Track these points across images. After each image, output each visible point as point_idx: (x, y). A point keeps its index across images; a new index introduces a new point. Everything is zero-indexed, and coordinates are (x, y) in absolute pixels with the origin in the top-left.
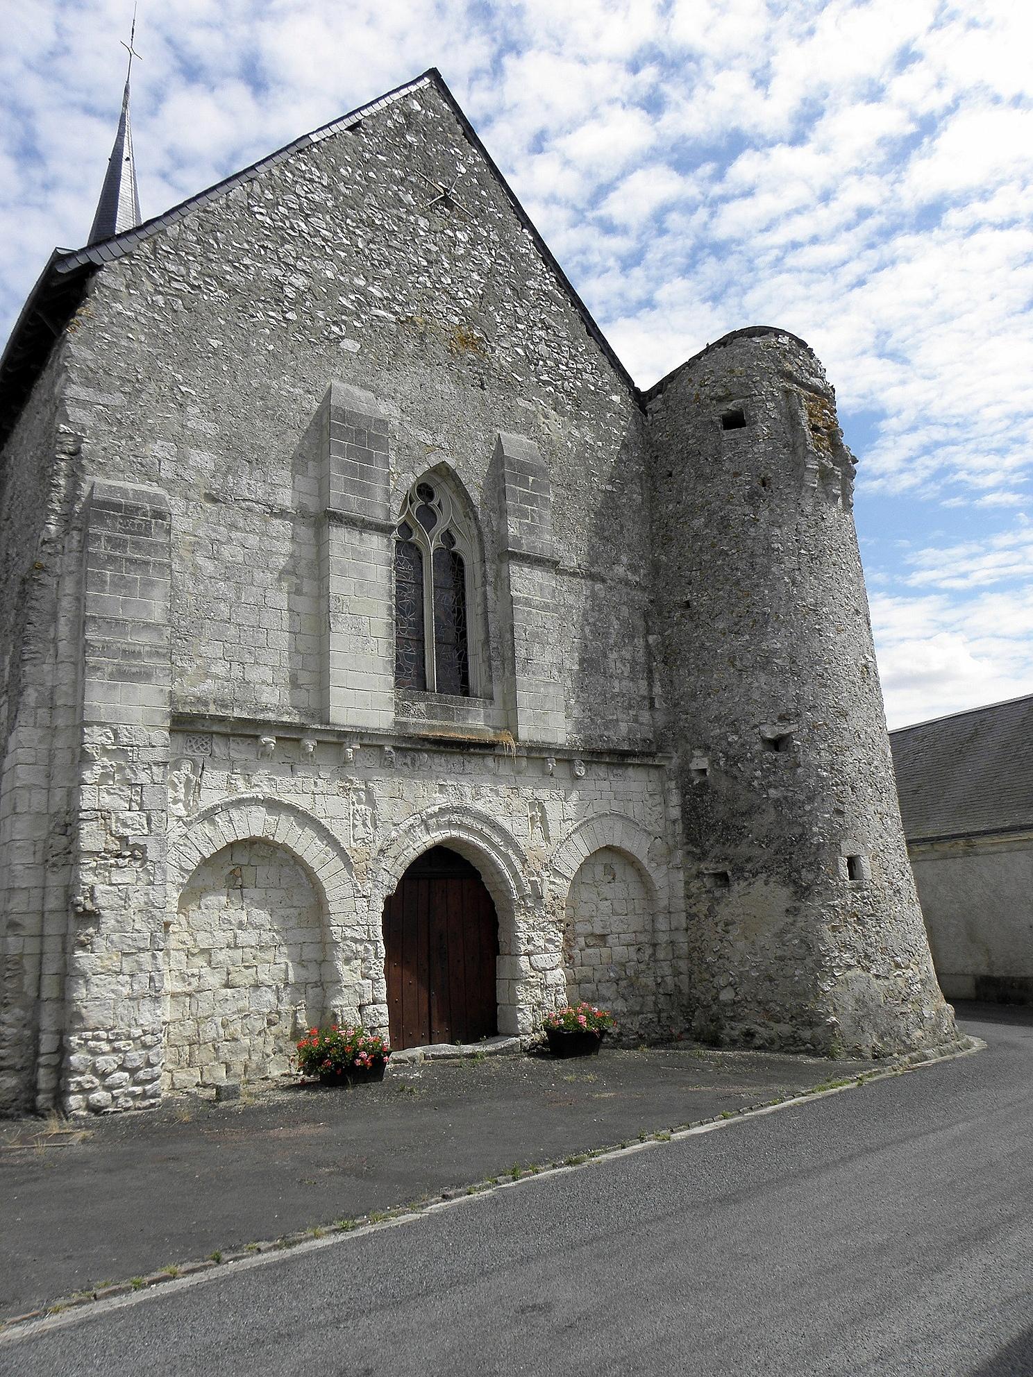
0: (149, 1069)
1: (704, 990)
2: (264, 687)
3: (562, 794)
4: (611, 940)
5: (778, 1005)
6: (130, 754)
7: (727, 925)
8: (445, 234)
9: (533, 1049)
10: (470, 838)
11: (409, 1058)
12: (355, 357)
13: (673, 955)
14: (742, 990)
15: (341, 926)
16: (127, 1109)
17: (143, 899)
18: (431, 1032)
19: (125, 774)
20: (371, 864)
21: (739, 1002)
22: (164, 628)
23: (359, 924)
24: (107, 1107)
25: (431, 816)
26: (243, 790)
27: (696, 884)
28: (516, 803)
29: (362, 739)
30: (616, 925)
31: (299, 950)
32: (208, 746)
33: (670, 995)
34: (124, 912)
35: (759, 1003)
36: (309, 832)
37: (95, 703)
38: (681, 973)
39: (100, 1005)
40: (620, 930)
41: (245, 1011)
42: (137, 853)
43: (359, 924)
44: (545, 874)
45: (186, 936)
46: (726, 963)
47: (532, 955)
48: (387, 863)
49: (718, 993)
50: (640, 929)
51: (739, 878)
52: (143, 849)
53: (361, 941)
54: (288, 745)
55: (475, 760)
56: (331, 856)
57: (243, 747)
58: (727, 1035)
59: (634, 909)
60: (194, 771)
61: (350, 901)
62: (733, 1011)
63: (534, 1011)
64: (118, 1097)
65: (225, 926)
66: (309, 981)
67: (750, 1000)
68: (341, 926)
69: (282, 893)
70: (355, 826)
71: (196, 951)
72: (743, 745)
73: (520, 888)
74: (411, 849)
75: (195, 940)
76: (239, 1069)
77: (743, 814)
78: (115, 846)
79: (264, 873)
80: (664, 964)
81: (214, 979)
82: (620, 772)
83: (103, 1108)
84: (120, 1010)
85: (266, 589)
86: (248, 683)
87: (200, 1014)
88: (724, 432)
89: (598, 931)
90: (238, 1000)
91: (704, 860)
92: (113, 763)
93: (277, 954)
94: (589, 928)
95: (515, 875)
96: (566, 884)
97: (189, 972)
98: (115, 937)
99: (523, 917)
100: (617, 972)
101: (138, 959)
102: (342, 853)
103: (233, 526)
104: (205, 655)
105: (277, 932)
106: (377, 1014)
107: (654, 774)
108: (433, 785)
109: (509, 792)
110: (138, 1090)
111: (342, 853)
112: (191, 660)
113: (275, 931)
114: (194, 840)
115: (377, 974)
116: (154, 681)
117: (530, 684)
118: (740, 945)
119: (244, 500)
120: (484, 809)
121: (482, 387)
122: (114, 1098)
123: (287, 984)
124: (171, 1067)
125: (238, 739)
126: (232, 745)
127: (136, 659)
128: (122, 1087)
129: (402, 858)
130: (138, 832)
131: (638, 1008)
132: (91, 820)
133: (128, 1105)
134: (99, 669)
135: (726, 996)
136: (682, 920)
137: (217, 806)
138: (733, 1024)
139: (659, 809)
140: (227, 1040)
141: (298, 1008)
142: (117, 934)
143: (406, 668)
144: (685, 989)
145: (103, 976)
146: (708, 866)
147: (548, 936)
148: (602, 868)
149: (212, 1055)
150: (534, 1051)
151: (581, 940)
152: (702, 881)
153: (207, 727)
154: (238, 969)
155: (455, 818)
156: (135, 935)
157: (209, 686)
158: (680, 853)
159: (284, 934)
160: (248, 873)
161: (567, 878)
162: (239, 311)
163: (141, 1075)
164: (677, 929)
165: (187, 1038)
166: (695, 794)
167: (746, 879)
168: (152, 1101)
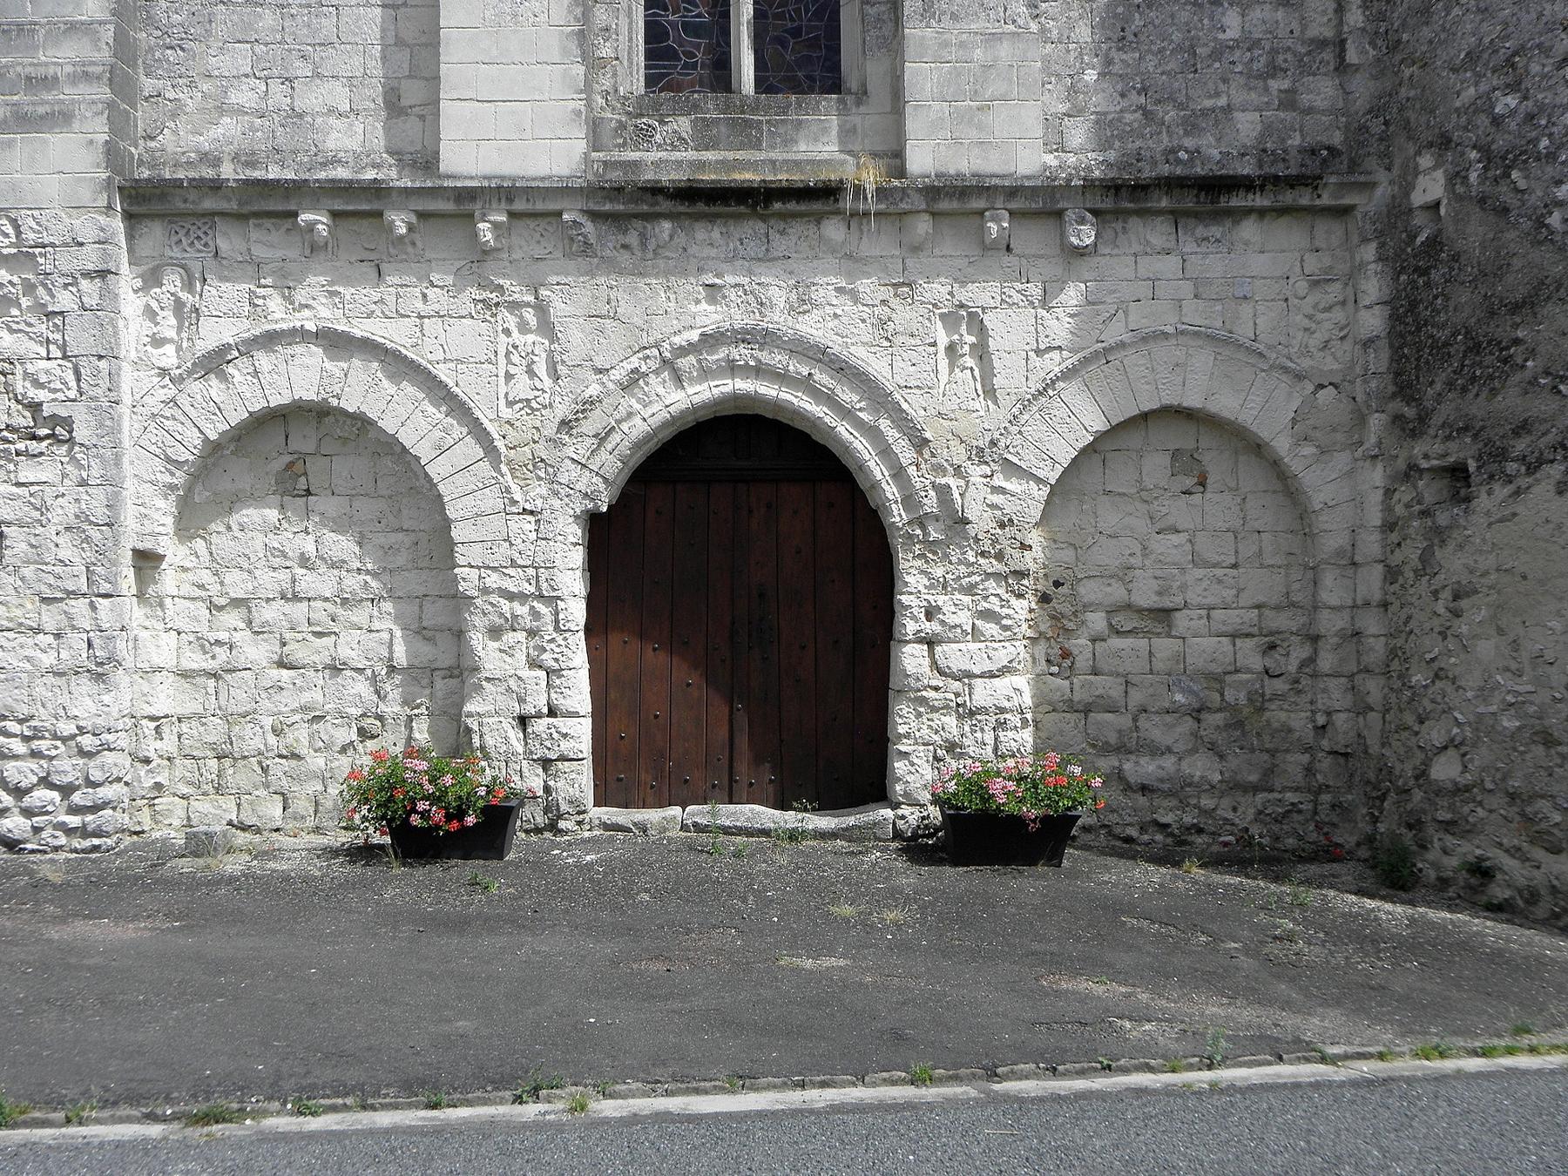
0: (90, 790)
1: (1402, 751)
2: (332, 121)
3: (1035, 290)
4: (1181, 621)
5: (1557, 807)
6: (41, 260)
7: (1456, 597)
9: (930, 836)
10: (783, 396)
11: (635, 824)
14: (1481, 757)
15: (479, 568)
16: (56, 849)
17: (72, 509)
18: (731, 781)
19: (36, 297)
20: (542, 451)
21: (1468, 789)
23: (514, 564)
24: (25, 841)
25: (682, 351)
26: (278, 316)
27: (1404, 494)
28: (904, 316)
29: (510, 200)
30: (1199, 587)
32: (208, 239)
33: (1346, 755)
34: (39, 530)
35: (1513, 797)
36: (409, 388)
39: (7, 680)
40: (1210, 600)
41: (315, 709)
42: (56, 431)
43: (514, 564)
44: (976, 472)
45: (206, 577)
46: (1450, 689)
47: (940, 642)
48: (576, 448)
49: (1427, 763)
51: (1491, 477)
52: (68, 423)
53: (522, 597)
54: (353, 225)
55: (797, 229)
57: (276, 236)
58: (1432, 864)
59: (1260, 553)
60: (189, 286)
61: (497, 522)
62: (1451, 808)
63: (937, 759)
64: (41, 829)
65: (277, 562)
66: (437, 665)
67: (1489, 786)
68: (479, 568)
70: (509, 377)
71: (222, 601)
72: (1530, 117)
73: (909, 500)
74: (637, 420)
75: (222, 583)
76: (302, 805)
77: (1516, 308)
78: (24, 420)
79: (347, 468)
80: (1332, 683)
81: (257, 652)
82: (1215, 231)
83: (20, 842)
84: (40, 691)
86: (300, 116)
87: (232, 708)
89: (1145, 596)
90: (301, 689)
91: (1422, 433)
92: (15, 279)
93: (376, 613)
94: (1117, 593)
95: (899, 473)
96: (1035, 492)
97: (212, 637)
98: (28, 572)
99: (918, 563)
100: (1192, 692)
101: (65, 608)
102: (478, 431)
104: (216, 73)
105: (375, 575)
106: (555, 735)
107: (1329, 232)
108: (691, 286)
109: (886, 293)
110: (74, 821)
111: (478, 431)
113: (368, 572)
114: (188, 409)
115: (556, 660)
116: (76, 126)
117: (946, 44)
118: (1486, 649)
120: (820, 333)
122: (37, 830)
123: (392, 669)
124: (185, 790)
125: (268, 223)
126: (255, 235)
127: (49, 90)
128: (47, 813)
129: (616, 438)
130: (60, 396)
131: (1253, 778)
133: (57, 843)
135: (1445, 770)
136: (1371, 582)
137: (226, 348)
138: (1450, 841)
139: (1339, 315)
140: (281, 756)
141: (416, 711)
142: (32, 567)
144: (1375, 749)
145: (11, 635)
146: (1429, 450)
148: (1165, 459)
149: (259, 778)
150: (917, 848)
151: (1097, 621)
152: (1415, 487)
153: (193, 202)
154: (300, 637)
155: (741, 353)
156: (58, 569)
157: (227, 130)
158: (1376, 422)
159: (386, 577)
160: (315, 466)
161: (1039, 480)
163: (77, 798)
164: (1367, 604)
165: (212, 746)
167: (1509, 480)
168: (96, 841)
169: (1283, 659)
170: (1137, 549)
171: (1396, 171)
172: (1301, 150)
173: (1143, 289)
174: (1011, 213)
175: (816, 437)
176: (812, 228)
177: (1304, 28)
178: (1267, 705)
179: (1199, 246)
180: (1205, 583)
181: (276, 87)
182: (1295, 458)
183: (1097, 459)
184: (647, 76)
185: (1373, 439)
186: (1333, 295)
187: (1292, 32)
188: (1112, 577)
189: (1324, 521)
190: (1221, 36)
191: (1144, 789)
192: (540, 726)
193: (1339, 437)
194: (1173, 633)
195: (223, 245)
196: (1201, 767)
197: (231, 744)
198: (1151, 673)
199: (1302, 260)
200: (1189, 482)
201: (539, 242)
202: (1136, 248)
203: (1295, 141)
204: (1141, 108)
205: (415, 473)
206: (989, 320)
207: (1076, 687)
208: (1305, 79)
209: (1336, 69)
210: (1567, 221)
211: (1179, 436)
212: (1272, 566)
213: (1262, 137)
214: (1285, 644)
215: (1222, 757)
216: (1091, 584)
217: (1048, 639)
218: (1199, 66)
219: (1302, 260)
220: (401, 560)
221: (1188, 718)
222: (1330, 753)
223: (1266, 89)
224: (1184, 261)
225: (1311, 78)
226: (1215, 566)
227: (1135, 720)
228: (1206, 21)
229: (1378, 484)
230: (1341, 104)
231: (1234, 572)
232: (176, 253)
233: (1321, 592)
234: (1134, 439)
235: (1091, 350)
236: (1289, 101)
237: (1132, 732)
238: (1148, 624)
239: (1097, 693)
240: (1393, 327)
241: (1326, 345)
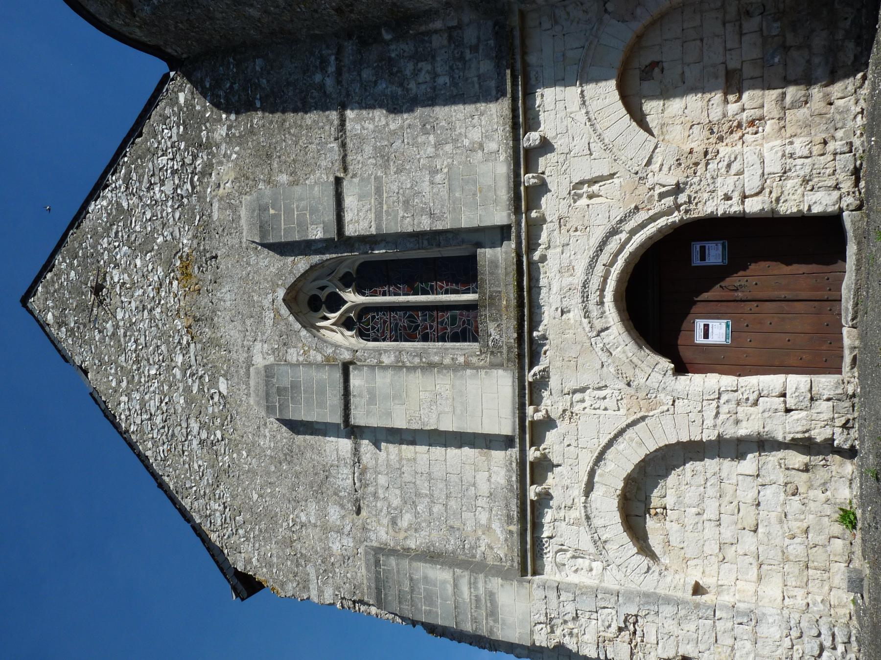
2: (493, 480)
4: (733, 65)
8: (120, 293)
12: (229, 382)
15: (702, 429)
17: (670, 621)
20: (642, 395)
22: (456, 574)
37: (517, 635)
44: (651, 180)
56: (634, 435)
73: (668, 212)
78: (626, 635)
81: (749, 542)
85: (416, 473)
86: (491, 494)
90: (769, 523)
95: (653, 219)
103: (375, 495)
112: (478, 539)
114: (622, 560)
119: (355, 484)
121: (216, 257)
124: (827, 588)
132: (606, 652)
134: (491, 629)
143: (463, 325)
147: (723, 171)
155: (594, 298)
162: (229, 476)
163: (828, 643)
165: (801, 572)
223: (470, 60)
236: (474, 49)
241: (586, 12)
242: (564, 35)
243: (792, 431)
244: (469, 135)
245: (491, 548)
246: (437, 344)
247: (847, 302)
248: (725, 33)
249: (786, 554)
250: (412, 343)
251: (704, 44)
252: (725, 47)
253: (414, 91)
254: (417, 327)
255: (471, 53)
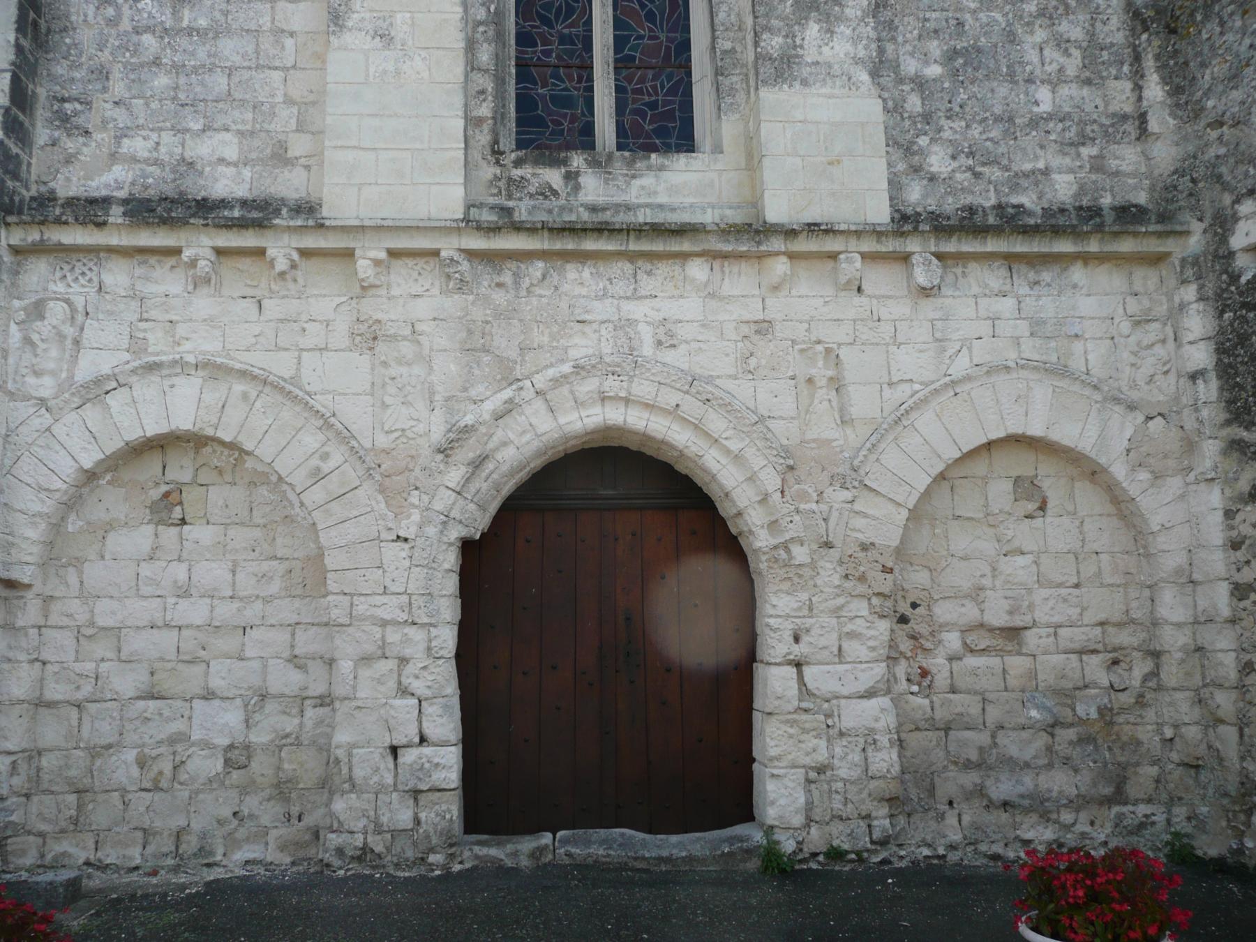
2: (222, 169)
13: (1204, 678)
15: (350, 594)
31: (288, 636)
38: (1222, 721)
40: (1056, 619)
47: (808, 663)
50: (1117, 617)
66: (310, 693)
69: (257, 533)
80: (1179, 695)
88: (1146, 741)
89: (997, 616)
94: (970, 613)
107: (1146, 278)
129: (490, 466)
136: (1220, 599)
143: (552, 121)
148: (1008, 486)
158: (1211, 450)
166: (1244, 305)
169: (1126, 674)
170: (988, 570)
171: (1208, 221)
172: (1114, 208)
173: (984, 328)
174: (864, 256)
175: (680, 468)
176: (677, 268)
177: (1106, 106)
178: (1115, 719)
179: (1031, 289)
180: (1051, 603)
181: (167, 137)
182: (1134, 483)
183: (945, 485)
184: (517, 140)
185: (1208, 464)
186: (1153, 334)
187: (1096, 107)
188: (965, 597)
189: (1162, 542)
190: (1035, 109)
191: (1006, 805)
192: (408, 757)
193: (1171, 463)
194: (1024, 651)
195: (108, 279)
196: (1059, 782)
197: (92, 777)
198: (1006, 690)
199: (1124, 303)
200: (1031, 507)
201: (416, 280)
202: (975, 290)
203: (1106, 201)
204: (969, 168)
205: (290, 502)
206: (843, 353)
207: (937, 706)
208: (1111, 147)
209: (1138, 139)
210: (1255, 315)
211: (1022, 464)
212: (1112, 585)
213: (1077, 195)
214: (1128, 659)
215: (1076, 771)
216: (947, 605)
217: (907, 659)
218: (1018, 134)
219: (1124, 303)
220: (275, 587)
221: (1044, 734)
222: (1179, 765)
223: (1079, 155)
224: (1020, 302)
225: (1116, 146)
226: (1060, 585)
227: (993, 736)
228: (1022, 96)
229: (1217, 505)
230: (1143, 169)
231: (1076, 592)
232: (60, 287)
233: (1159, 609)
234: (979, 467)
235: (942, 382)
236: (1098, 165)
237: (991, 748)
238: (999, 642)
239: (956, 711)
240: (1220, 360)
241: (1151, 380)
242: (1113, 338)
243: (355, 760)
244: (935, 148)
245: (68, 161)
246: (513, 63)
247: (603, 842)
248: (1087, 626)
249: (103, 751)
250: (513, 11)
251: (1071, 590)
252: (1060, 626)
253: (1028, 38)
254: (546, 21)
255: (1091, 157)
